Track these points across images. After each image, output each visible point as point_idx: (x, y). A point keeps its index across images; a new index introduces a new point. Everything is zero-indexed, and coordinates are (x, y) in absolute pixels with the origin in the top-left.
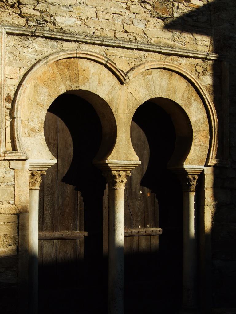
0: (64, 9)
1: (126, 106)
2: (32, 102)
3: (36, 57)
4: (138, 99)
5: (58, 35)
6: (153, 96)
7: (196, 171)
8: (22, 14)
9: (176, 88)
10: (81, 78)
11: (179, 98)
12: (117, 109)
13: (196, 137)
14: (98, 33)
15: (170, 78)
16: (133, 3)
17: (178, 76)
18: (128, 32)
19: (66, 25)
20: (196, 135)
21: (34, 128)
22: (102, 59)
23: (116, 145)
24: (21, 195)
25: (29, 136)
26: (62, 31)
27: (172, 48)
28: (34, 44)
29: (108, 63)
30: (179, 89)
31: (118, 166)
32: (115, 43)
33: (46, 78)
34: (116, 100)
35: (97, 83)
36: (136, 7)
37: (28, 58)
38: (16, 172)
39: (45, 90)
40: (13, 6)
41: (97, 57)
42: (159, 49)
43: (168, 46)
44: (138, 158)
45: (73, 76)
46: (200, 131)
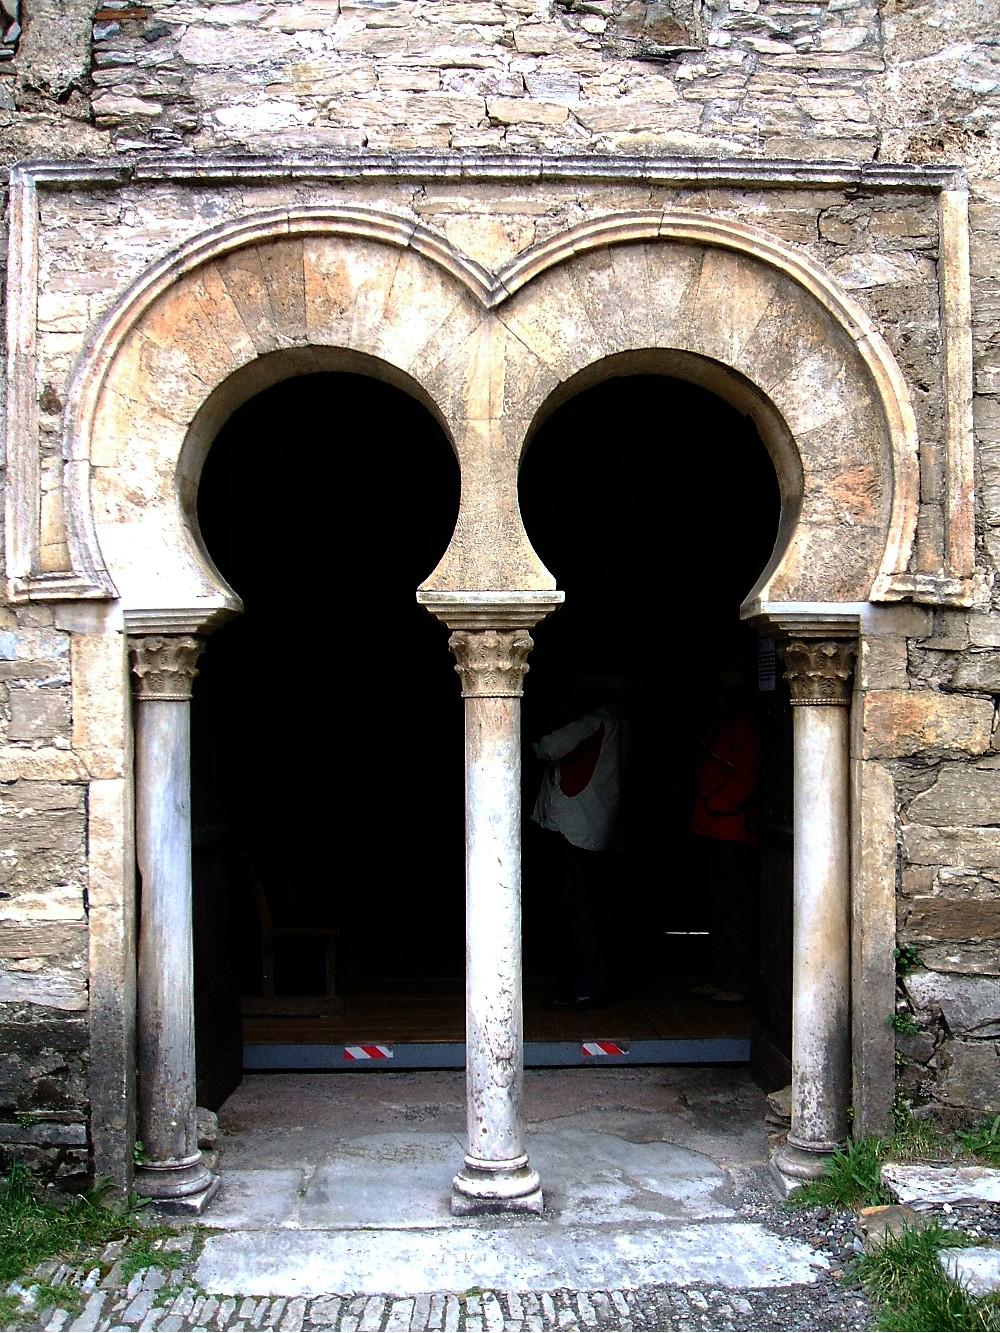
0: (247, 78)
1: (501, 390)
2: (132, 405)
3: (147, 252)
4: (550, 360)
5: (220, 168)
6: (616, 346)
7: (824, 627)
8: (99, 119)
9: (723, 308)
10: (315, 304)
11: (737, 347)
12: (461, 406)
13: (817, 490)
14: (381, 143)
15: (696, 274)
16: (531, 19)
17: (730, 267)
18: (507, 125)
19: (257, 131)
20: (818, 482)
21: (140, 492)
22: (392, 230)
23: (456, 536)
24: (95, 718)
25: (122, 520)
26: (240, 152)
27: (694, 160)
28: (141, 210)
29: (417, 240)
30: (736, 311)
31: (473, 612)
32: (446, 167)
33: (183, 318)
34: (457, 374)
35: (380, 314)
36: (548, 31)
37: (120, 258)
38: (78, 642)
39: (179, 359)
40: (64, 98)
41: (372, 225)
42: (640, 169)
43: (675, 155)
44: (552, 582)
45: (286, 302)
46: (837, 467)
